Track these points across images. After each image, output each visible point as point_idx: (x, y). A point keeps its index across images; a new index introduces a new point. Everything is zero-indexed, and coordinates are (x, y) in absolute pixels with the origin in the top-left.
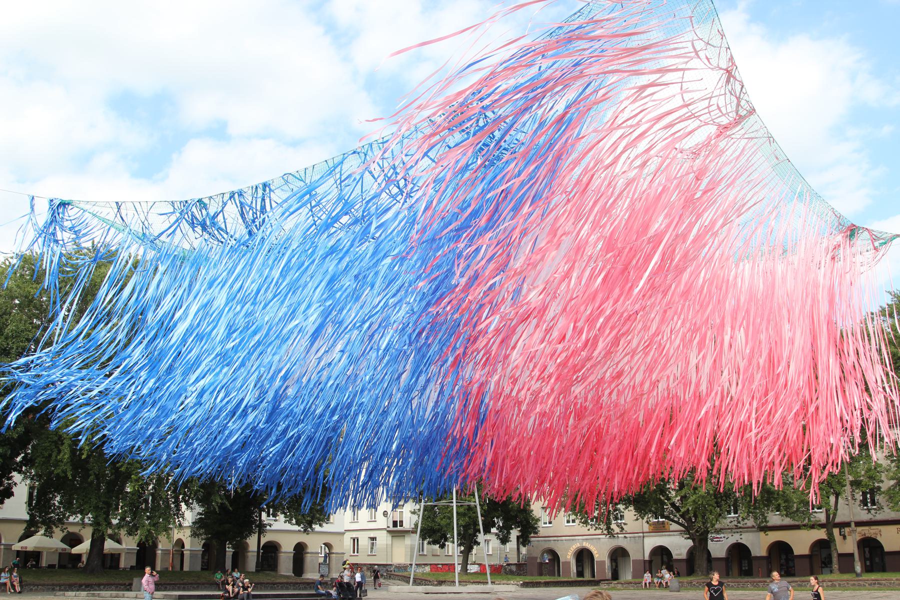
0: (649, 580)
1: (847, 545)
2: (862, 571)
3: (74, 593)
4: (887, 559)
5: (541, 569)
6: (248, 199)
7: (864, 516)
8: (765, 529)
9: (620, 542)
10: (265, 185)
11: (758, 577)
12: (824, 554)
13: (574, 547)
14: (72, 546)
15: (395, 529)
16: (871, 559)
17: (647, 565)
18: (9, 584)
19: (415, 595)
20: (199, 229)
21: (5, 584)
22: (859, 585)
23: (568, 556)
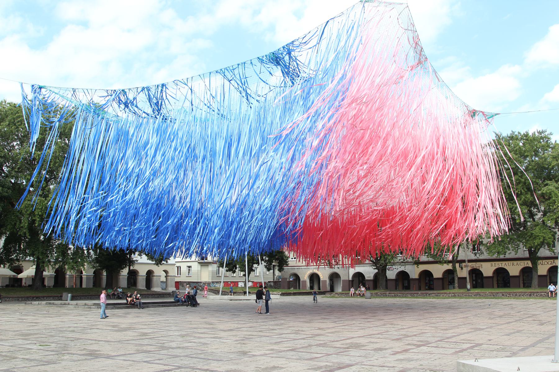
1: (463, 273)
2: (471, 288)
3: (37, 302)
4: (485, 280)
5: (290, 285)
6: (153, 91)
7: (473, 257)
8: (418, 263)
9: (336, 270)
10: (163, 85)
11: (413, 290)
12: (450, 277)
14: (19, 274)
16: (476, 281)
17: (351, 283)
19: (224, 301)
20: (123, 106)
22: (469, 296)
23: (305, 277)
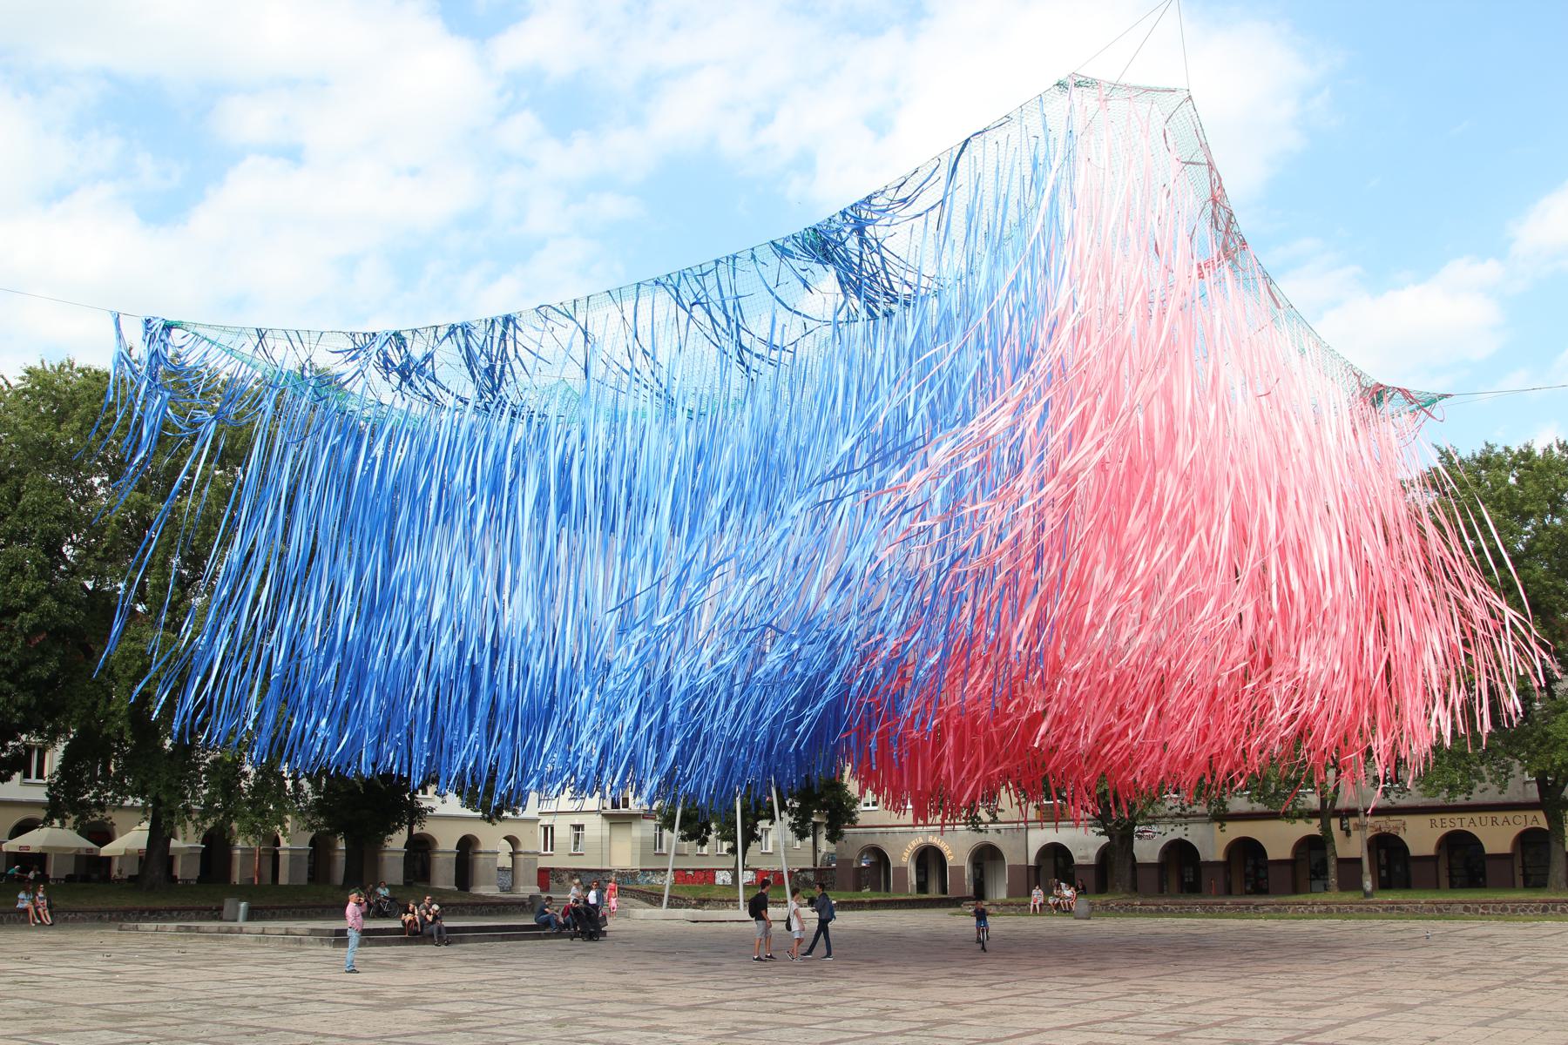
0: (1041, 900)
1: (1352, 845)
5: (859, 879)
6: (479, 336)
8: (1223, 817)
9: (990, 837)
10: (507, 320)
13: (914, 844)
15: (615, 811)
17: (1032, 873)
18: (32, 911)
20: (395, 378)
21: (26, 911)
23: (903, 856)
